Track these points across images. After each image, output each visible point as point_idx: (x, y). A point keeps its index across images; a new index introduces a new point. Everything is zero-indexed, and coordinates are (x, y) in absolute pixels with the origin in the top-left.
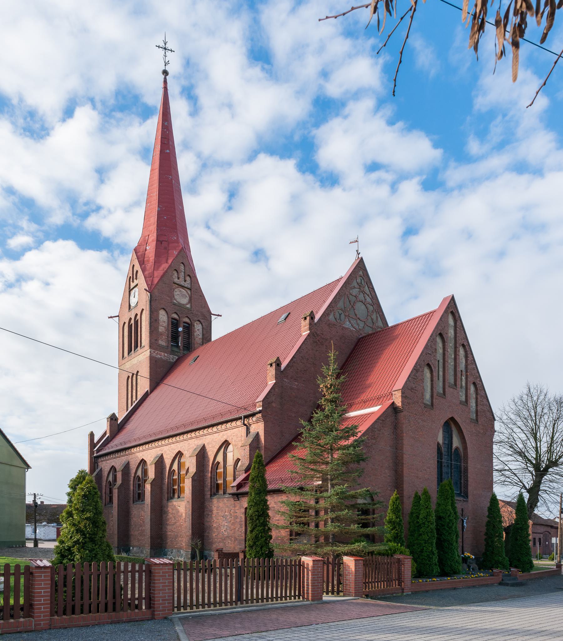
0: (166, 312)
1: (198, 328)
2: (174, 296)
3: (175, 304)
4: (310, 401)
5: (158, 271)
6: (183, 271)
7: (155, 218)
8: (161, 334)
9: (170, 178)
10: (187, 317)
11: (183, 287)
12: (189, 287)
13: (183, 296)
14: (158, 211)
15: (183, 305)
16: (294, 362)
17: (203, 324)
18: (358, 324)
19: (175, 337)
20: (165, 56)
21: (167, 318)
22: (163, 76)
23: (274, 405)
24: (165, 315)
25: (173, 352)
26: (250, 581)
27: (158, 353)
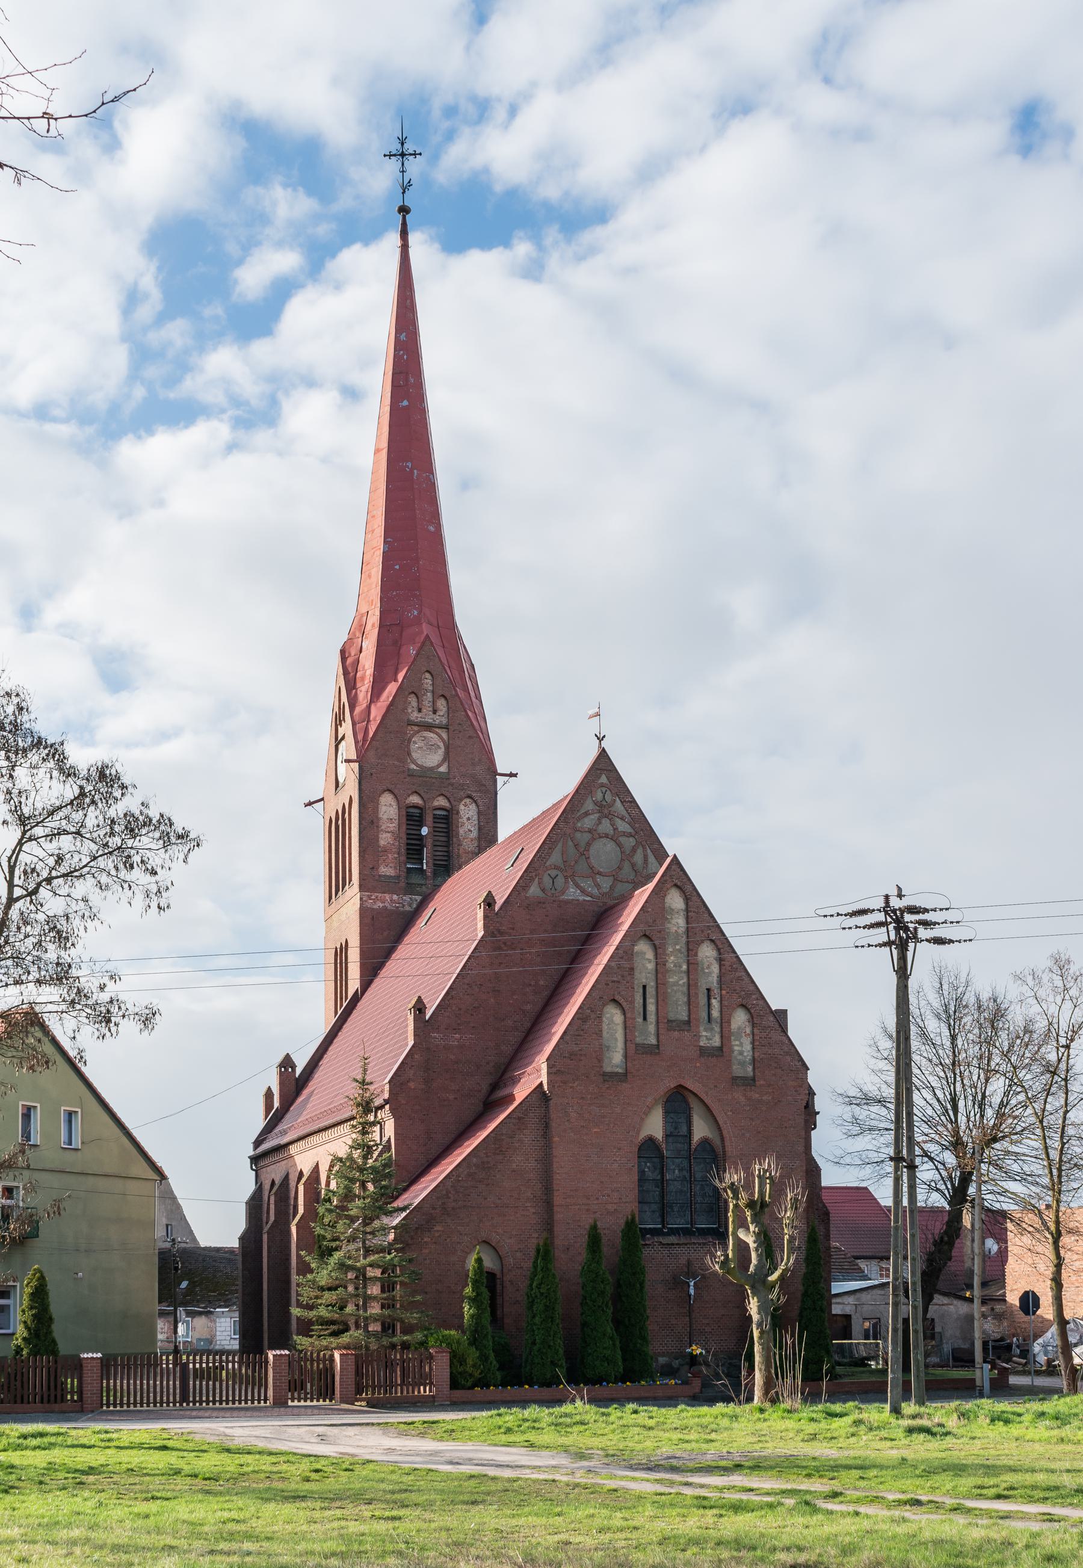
0: (396, 797)
1: (468, 814)
2: (409, 754)
3: (411, 774)
4: (488, 1063)
6: (431, 688)
7: (378, 572)
8: (385, 851)
9: (408, 467)
10: (442, 795)
11: (429, 727)
13: (433, 747)
15: (431, 769)
16: (452, 998)
17: (480, 803)
18: (598, 886)
19: (414, 848)
22: (400, 217)
23: (412, 1085)
24: (393, 803)
25: (410, 889)
26: (237, 1387)
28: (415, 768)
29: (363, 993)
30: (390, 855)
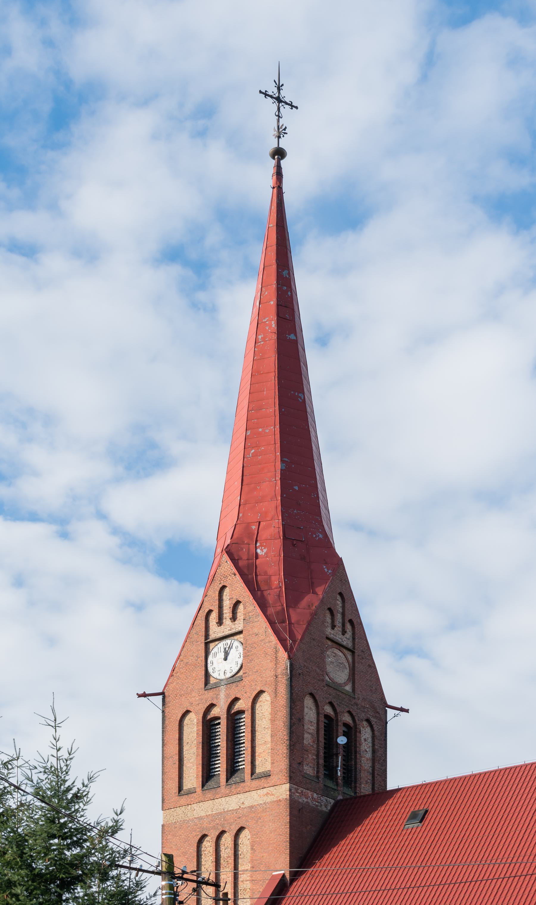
5: (298, 610)
9: (301, 398)
11: (339, 645)
12: (350, 645)
14: (281, 470)
20: (279, 116)
21: (315, 715)
22: (273, 162)
27: (302, 792)
28: (328, 680)
29: (292, 881)
30: (310, 755)
